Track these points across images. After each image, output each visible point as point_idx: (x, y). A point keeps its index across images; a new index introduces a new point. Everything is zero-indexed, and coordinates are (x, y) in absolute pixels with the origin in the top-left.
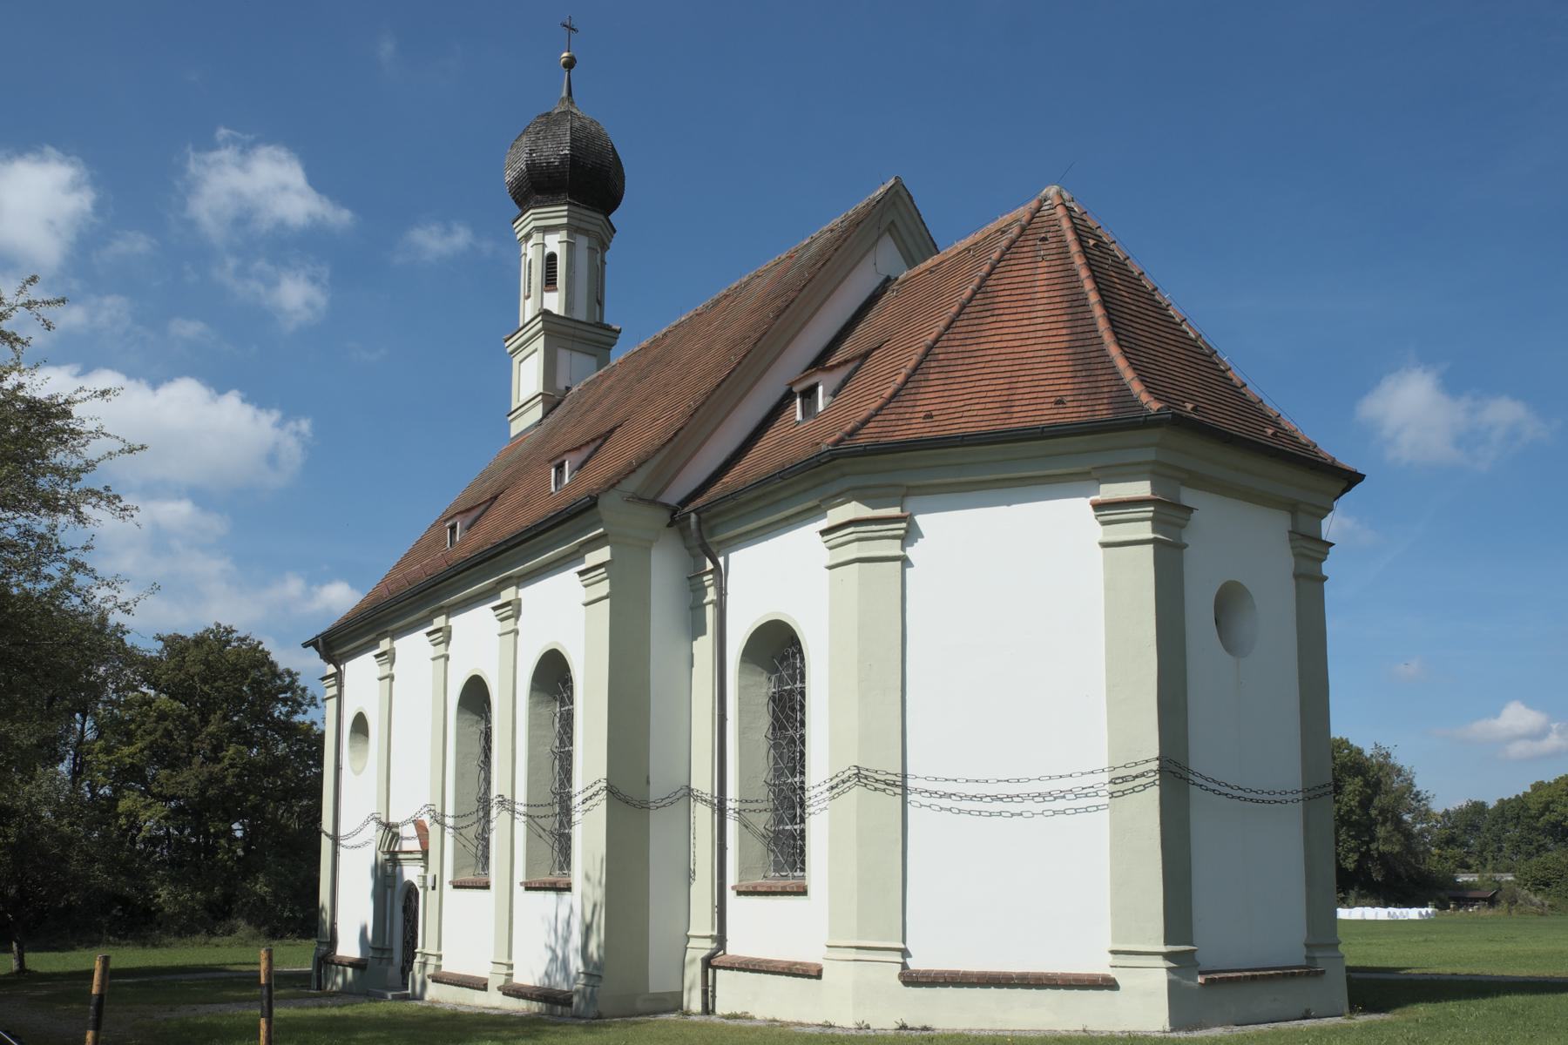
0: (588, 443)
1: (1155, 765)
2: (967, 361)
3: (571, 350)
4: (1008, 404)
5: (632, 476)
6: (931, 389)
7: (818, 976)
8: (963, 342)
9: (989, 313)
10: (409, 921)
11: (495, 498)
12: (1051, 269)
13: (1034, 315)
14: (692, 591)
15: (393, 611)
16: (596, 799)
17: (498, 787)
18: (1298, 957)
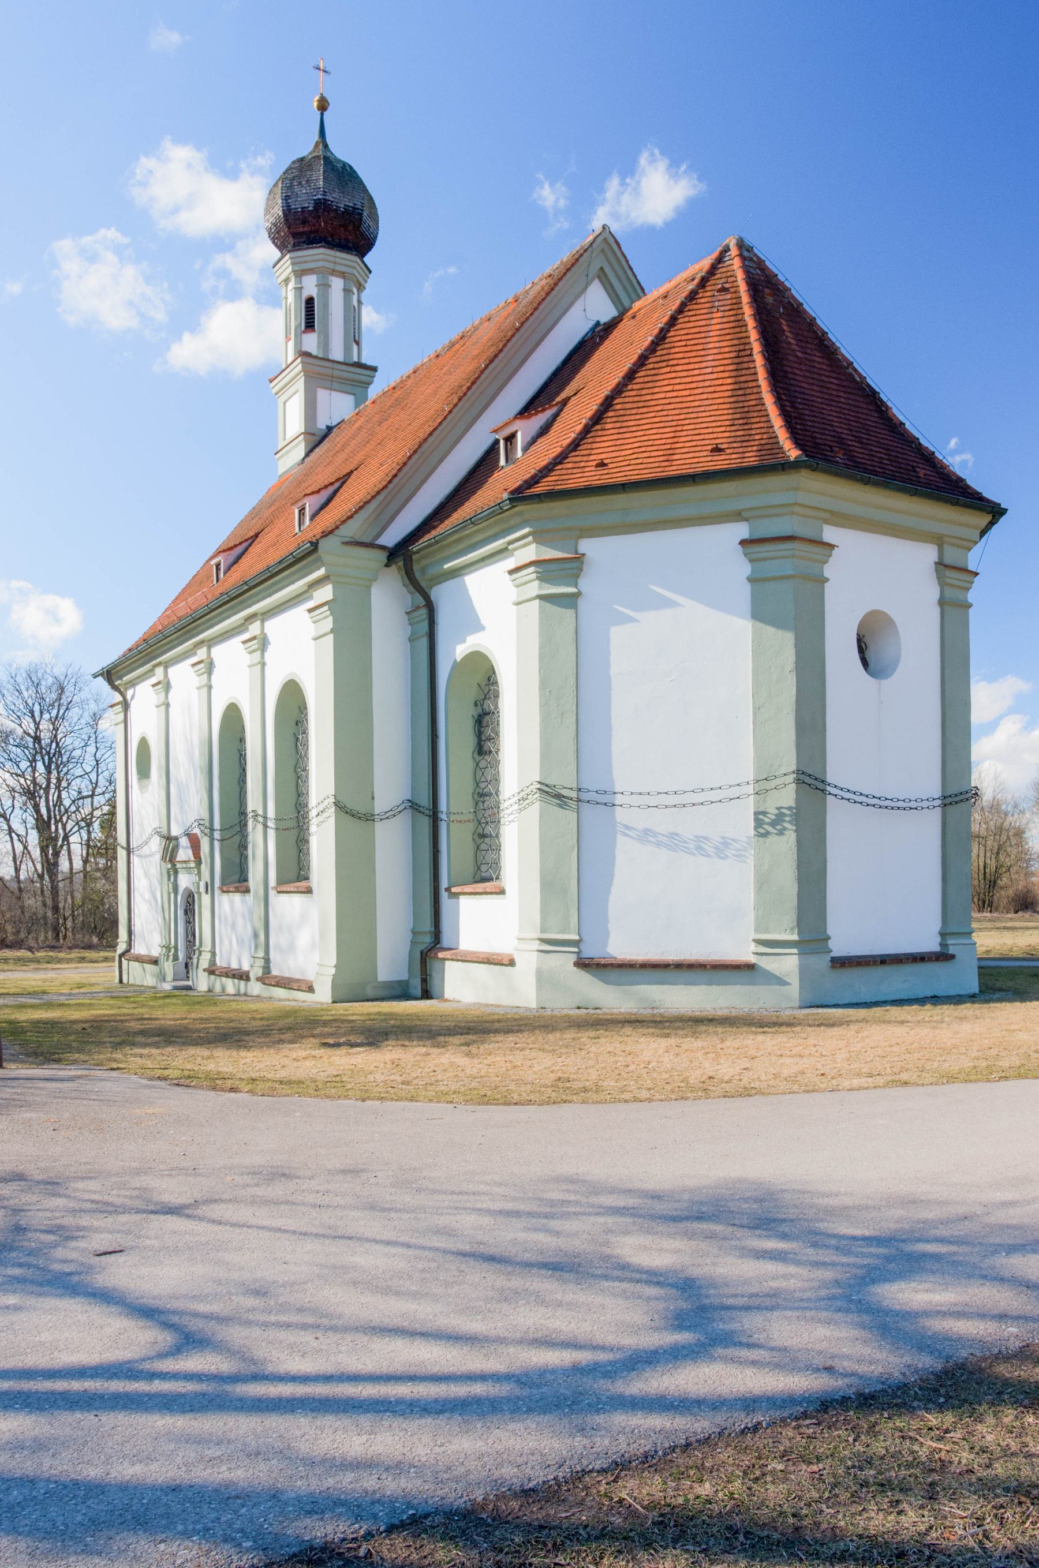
0: (326, 487)
1: (791, 778)
2: (641, 411)
3: (331, 389)
4: (671, 452)
5: (350, 522)
6: (605, 438)
7: (512, 963)
8: (639, 392)
9: (664, 364)
10: (189, 922)
11: (257, 535)
12: (724, 320)
13: (704, 365)
14: (411, 624)
15: (163, 645)
16: (325, 815)
17: (253, 803)
18: (931, 944)
